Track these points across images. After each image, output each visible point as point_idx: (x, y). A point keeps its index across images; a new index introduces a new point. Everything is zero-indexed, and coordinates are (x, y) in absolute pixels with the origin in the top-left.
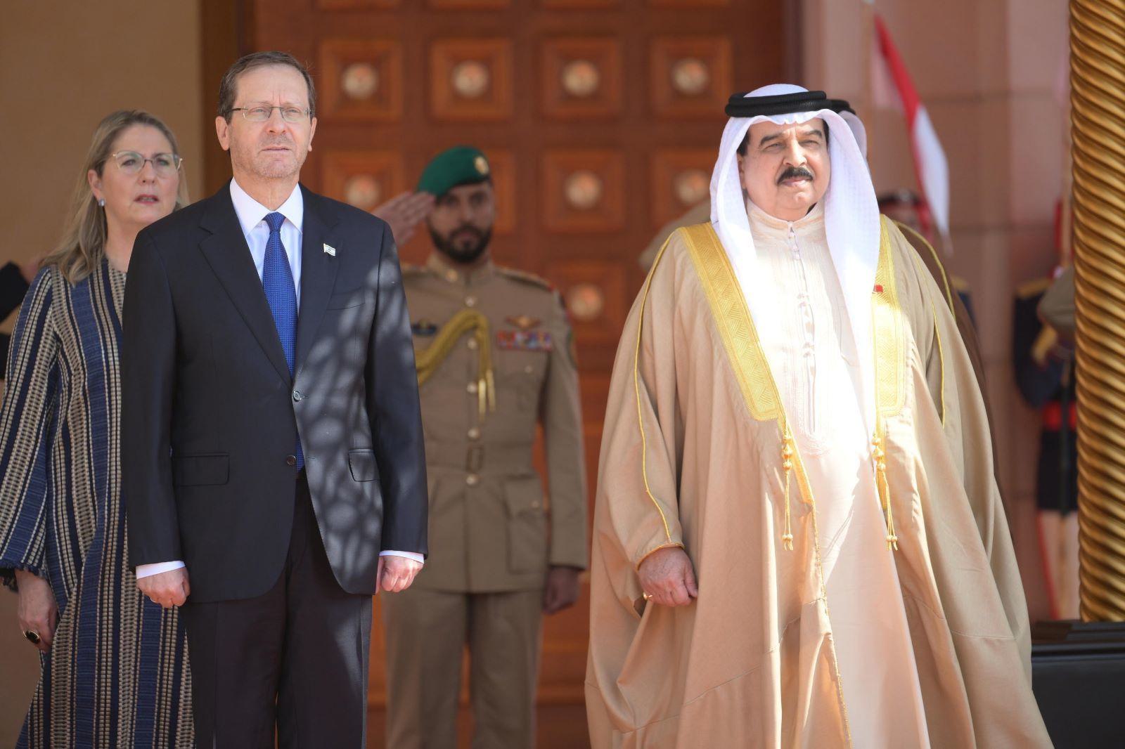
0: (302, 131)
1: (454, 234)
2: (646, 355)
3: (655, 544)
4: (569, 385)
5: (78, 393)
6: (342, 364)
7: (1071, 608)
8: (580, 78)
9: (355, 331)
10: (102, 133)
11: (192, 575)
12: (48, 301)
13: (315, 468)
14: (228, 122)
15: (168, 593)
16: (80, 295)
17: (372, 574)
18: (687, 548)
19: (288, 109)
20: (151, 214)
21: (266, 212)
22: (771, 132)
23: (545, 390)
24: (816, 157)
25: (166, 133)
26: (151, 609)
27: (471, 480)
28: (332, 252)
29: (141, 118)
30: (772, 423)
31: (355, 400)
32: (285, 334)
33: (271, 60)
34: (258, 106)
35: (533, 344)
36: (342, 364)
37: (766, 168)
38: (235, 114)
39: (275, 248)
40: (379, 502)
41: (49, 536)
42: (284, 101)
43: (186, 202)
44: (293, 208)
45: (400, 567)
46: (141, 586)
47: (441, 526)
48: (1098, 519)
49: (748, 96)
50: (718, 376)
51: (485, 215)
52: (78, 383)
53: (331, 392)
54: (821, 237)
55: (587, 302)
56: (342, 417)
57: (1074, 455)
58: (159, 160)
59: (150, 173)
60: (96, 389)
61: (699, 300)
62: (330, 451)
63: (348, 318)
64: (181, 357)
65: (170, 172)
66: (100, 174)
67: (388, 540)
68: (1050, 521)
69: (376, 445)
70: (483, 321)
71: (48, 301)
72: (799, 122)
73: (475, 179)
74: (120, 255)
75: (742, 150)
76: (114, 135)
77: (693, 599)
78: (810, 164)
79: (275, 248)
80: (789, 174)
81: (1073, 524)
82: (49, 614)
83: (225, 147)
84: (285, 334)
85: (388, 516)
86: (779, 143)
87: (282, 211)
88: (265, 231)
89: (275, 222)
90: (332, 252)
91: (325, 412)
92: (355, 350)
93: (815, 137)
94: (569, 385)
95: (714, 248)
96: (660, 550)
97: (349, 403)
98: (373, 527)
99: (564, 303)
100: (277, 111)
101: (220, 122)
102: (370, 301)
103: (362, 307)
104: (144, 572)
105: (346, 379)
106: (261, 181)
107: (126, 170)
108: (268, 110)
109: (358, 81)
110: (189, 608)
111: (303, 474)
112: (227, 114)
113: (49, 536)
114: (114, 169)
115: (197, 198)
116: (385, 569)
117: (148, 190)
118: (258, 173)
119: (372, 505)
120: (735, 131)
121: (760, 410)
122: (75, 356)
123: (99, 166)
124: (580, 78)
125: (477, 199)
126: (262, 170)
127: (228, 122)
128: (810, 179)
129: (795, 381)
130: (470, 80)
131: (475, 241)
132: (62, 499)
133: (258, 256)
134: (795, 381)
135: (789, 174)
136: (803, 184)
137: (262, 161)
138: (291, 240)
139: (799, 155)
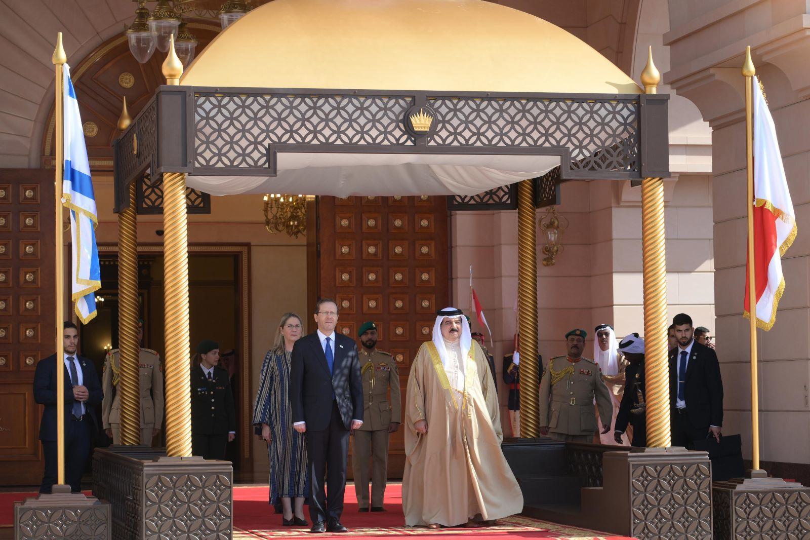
0: (335, 318)
1: (367, 341)
2: (417, 373)
3: (418, 419)
4: (396, 379)
5: (277, 381)
6: (342, 375)
7: (517, 434)
8: (399, 304)
9: (345, 367)
10: (284, 318)
11: (307, 425)
12: (271, 359)
13: (337, 398)
14: (317, 315)
15: (302, 429)
16: (278, 359)
17: (351, 423)
18: (426, 420)
19: (332, 313)
20: (295, 339)
21: (326, 337)
22: (448, 320)
23: (389, 378)
24: (459, 326)
25: (299, 319)
26: (295, 431)
27: (370, 404)
28: (342, 347)
29: (293, 315)
30: (448, 390)
31: (346, 383)
32: (330, 366)
33: (328, 301)
34: (324, 311)
35: (385, 370)
36: (342, 375)
37: (448, 328)
38: (319, 314)
39: (328, 346)
40: (352, 408)
41: (270, 415)
42: (331, 310)
43: (303, 336)
44: (333, 336)
45: (357, 423)
46: (295, 428)
47: (366, 413)
48: (525, 413)
49: (442, 310)
50: (435, 378)
51: (375, 337)
52: (278, 379)
53: (340, 381)
54: (459, 345)
55: (400, 358)
56: (343, 387)
57: (518, 398)
58: (297, 326)
59: (295, 329)
60: (282, 380)
61: (430, 360)
62: (340, 396)
63: (344, 363)
64: (305, 372)
65: (300, 329)
66: (283, 328)
67: (355, 417)
68: (512, 412)
69: (351, 393)
70: (372, 365)
71: (271, 359)
72: (455, 317)
73: (372, 328)
74: (290, 349)
75: (441, 324)
76: (286, 319)
77: (427, 432)
78: (457, 328)
79: (328, 346)
80: (453, 330)
81: (518, 412)
82: (270, 434)
83: (316, 321)
84: (330, 366)
85: (354, 411)
86: (450, 322)
87: (330, 337)
88: (326, 341)
89: (328, 339)
90: (342, 347)
91: (338, 387)
92: (346, 371)
93: (459, 321)
94: (396, 379)
95: (434, 348)
96: (420, 420)
97: (345, 383)
98: (351, 414)
99: (394, 359)
100: (329, 313)
101: (315, 315)
102: (350, 360)
103: (347, 361)
104: (296, 424)
105: (343, 379)
106: (325, 331)
107: (289, 328)
108: (327, 313)
109: (346, 304)
110: (307, 433)
111: (335, 400)
112: (317, 313)
113: (270, 415)
114: (286, 327)
115: (307, 335)
116: (353, 423)
117: (294, 333)
118: (324, 329)
119: (350, 408)
120: (439, 319)
121: (445, 387)
122: (277, 372)
123: (283, 326)
124: (399, 304)
125: (372, 333)
126: (325, 328)
127: (317, 315)
128: (457, 331)
129: (453, 380)
130: (372, 304)
131: (372, 343)
132: (273, 406)
133: (324, 348)
134: (453, 380)
135: (453, 330)
136: (456, 333)
137: (326, 325)
138: (332, 344)
139: (455, 325)
